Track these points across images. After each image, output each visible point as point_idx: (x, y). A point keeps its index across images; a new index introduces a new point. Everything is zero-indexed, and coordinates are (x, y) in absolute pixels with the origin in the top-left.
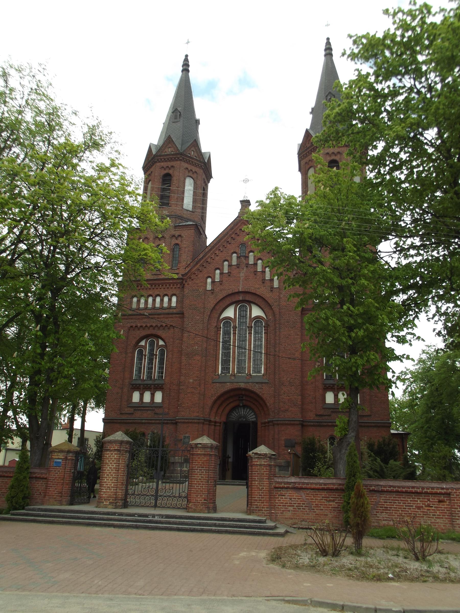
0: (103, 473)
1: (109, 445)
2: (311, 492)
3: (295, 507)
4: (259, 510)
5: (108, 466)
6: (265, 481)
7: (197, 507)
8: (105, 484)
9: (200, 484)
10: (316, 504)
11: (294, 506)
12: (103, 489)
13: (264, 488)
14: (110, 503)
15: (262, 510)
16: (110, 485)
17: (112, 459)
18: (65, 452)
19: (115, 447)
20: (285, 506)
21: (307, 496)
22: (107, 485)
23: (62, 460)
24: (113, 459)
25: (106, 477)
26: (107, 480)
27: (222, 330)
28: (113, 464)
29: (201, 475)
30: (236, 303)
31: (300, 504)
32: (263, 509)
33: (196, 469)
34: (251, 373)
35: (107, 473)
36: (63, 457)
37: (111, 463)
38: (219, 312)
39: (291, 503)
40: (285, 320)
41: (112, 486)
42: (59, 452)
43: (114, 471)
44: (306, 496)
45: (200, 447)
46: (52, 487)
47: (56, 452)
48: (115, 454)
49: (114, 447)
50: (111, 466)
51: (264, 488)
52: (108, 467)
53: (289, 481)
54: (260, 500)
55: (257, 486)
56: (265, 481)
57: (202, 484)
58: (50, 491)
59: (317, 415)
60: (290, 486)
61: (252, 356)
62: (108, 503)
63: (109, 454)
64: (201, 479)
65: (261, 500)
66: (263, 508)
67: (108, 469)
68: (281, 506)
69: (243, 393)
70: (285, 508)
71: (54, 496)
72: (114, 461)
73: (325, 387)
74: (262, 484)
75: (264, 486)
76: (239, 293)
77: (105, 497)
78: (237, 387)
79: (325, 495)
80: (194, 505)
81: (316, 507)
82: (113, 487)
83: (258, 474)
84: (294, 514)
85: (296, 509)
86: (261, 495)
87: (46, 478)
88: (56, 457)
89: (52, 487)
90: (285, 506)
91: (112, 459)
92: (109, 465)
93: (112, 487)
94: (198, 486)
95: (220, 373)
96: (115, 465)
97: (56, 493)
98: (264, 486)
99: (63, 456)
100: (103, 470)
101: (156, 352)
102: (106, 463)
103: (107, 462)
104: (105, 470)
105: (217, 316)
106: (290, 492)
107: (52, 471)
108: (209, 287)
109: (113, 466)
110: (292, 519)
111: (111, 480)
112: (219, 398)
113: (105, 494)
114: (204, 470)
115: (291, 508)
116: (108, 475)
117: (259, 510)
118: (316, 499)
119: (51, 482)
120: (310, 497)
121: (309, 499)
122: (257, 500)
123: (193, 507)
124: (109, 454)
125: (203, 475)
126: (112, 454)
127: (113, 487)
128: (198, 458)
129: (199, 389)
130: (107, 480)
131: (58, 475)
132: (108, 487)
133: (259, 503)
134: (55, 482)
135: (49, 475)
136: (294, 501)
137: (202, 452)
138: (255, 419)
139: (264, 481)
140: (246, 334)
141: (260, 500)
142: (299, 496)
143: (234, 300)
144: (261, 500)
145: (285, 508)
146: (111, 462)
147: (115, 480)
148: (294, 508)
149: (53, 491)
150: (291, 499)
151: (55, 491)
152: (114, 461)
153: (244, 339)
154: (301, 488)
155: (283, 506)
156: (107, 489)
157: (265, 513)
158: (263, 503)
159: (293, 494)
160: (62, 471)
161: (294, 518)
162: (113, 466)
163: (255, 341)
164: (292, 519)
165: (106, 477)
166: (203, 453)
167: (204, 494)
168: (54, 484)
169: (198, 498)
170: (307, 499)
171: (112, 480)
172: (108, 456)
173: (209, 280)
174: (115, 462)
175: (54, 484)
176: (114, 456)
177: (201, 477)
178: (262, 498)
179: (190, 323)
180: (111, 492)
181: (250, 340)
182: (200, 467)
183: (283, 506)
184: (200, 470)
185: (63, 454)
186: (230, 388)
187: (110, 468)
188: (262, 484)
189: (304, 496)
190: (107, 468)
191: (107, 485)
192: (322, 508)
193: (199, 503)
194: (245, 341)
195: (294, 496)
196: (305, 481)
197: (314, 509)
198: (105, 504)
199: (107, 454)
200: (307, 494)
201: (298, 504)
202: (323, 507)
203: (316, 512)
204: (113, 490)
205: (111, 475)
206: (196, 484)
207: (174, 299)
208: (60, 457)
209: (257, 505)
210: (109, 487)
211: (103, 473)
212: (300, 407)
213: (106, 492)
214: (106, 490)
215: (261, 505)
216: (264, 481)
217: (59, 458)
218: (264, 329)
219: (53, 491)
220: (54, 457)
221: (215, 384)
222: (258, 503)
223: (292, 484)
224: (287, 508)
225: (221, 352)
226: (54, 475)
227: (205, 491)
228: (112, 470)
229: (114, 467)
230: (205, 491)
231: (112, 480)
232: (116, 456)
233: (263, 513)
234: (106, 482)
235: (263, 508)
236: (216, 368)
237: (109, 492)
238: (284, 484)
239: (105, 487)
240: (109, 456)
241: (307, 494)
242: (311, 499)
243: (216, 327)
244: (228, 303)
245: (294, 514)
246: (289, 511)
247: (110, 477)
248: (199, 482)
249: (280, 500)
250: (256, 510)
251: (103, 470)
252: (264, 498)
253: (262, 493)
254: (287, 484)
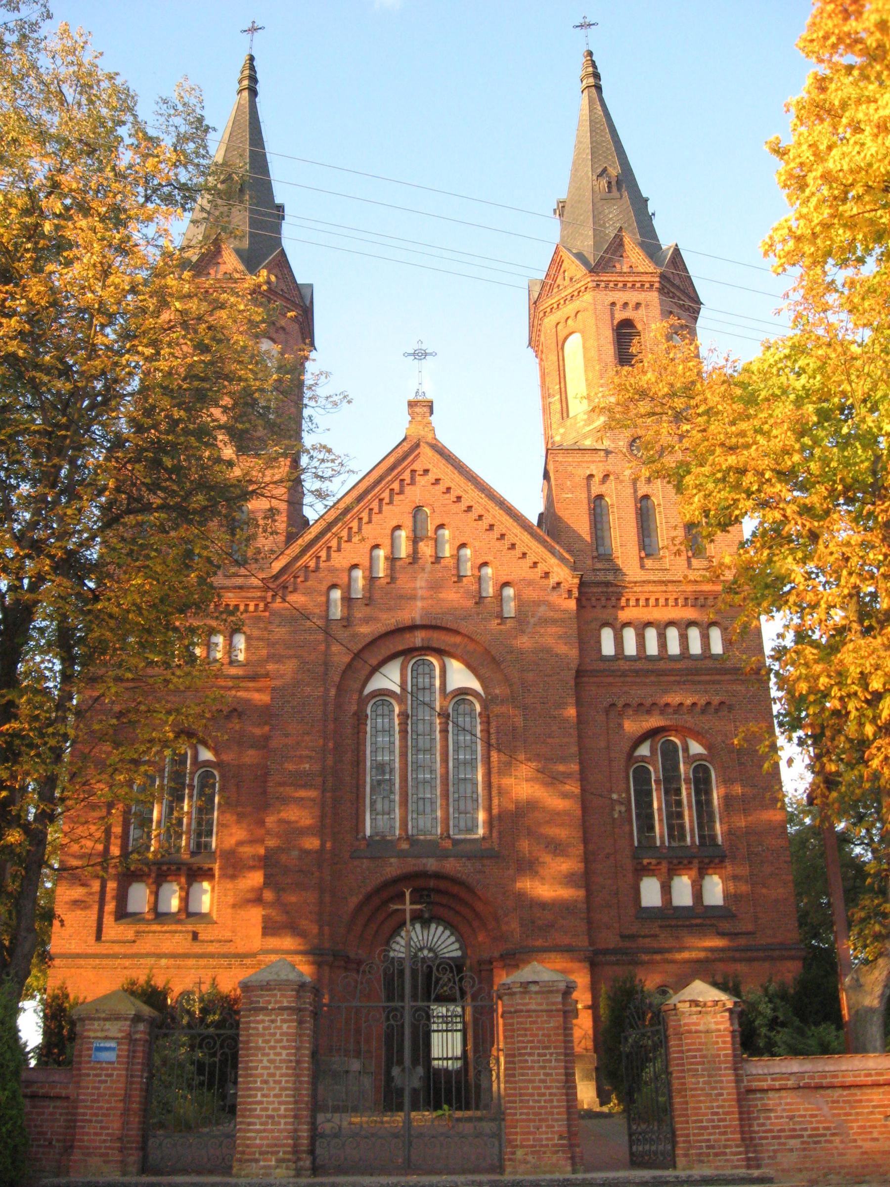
0: (251, 1075)
1: (262, 996)
2: (841, 1096)
3: (805, 1139)
4: (716, 1154)
5: (264, 1055)
6: (725, 1075)
7: (539, 1159)
8: (258, 1107)
9: (544, 1095)
10: (860, 1127)
11: (802, 1136)
12: (254, 1124)
13: (722, 1094)
14: (279, 1161)
15: (725, 1154)
16: (274, 1109)
17: (275, 1034)
18: (126, 1019)
19: (280, 1002)
20: (779, 1137)
21: (836, 1108)
22: (267, 1109)
23: (119, 1044)
24: (278, 1037)
25: (261, 1089)
26: (263, 1096)
27: (369, 722)
28: (278, 1050)
29: (544, 1068)
30: (407, 653)
31: (817, 1129)
32: (728, 1150)
33: (530, 1054)
34: (451, 833)
35: (262, 1075)
36: (120, 1035)
37: (274, 1048)
38: (363, 677)
39: (794, 1130)
40: (534, 697)
41: (282, 1112)
42: (105, 1019)
43: (284, 1071)
44: (832, 1108)
45: (536, 993)
46: (91, 1121)
47: (99, 1019)
48: (283, 1021)
49: (276, 1002)
50: (272, 1057)
51: (722, 1094)
52: (265, 1059)
53: (784, 1070)
54: (714, 1127)
55: (703, 1089)
56: (725, 1075)
57: (551, 1094)
58: (88, 1134)
59: (623, 937)
60: (790, 1083)
61: (451, 789)
62: (273, 1163)
63: (263, 1021)
64: (544, 1081)
65: (718, 1127)
66: (725, 1146)
67: (265, 1063)
68: (766, 1138)
69: (432, 883)
70: (780, 1144)
71: (100, 1148)
72: (281, 1041)
73: (639, 867)
74: (716, 1082)
75: (722, 1088)
76: (413, 628)
77: (261, 1146)
78: (416, 868)
79: (881, 1100)
80: (533, 1153)
81: (860, 1134)
82: (285, 1117)
83: (701, 1057)
84: (805, 1157)
85: (808, 1143)
86: (717, 1114)
87: (67, 1098)
88: (99, 1034)
89: (91, 1121)
90: (779, 1137)
91: (275, 1034)
92: (268, 1054)
93: (279, 1116)
94: (539, 1101)
95: (368, 832)
96: (284, 1052)
97: (105, 1141)
98: (722, 1088)
99: (121, 1031)
100: (251, 1068)
101: (192, 779)
102: (258, 1048)
103: (260, 1044)
104: (256, 1068)
105: (357, 686)
106: (789, 1100)
107: (88, 1075)
108: (337, 612)
109: (279, 1054)
110: (800, 1170)
111: (275, 1096)
112: (368, 898)
113: (262, 1138)
114: (551, 1054)
115: (792, 1143)
116: (266, 1082)
117: (716, 1154)
118: (857, 1114)
119: (86, 1107)
120: (842, 1108)
121: (839, 1115)
122: (706, 1128)
123: (530, 1158)
124: (263, 1021)
125: (550, 1068)
126: (272, 1021)
127: (285, 1117)
128: (532, 1023)
129: (317, 874)
130: (263, 1096)
131: (106, 1088)
132: (269, 1117)
133: (714, 1134)
134: (101, 1108)
135: (79, 1087)
136: (800, 1123)
137: (541, 1004)
138: (458, 953)
139: (720, 1075)
140: (432, 731)
141: (714, 1127)
142: (812, 1109)
143: (401, 647)
144: (718, 1127)
145: (780, 1144)
146: (272, 1044)
147: (287, 1096)
148: (803, 1143)
149: (96, 1134)
150: (791, 1118)
151: (101, 1134)
152: (281, 1041)
153: (428, 746)
154: (819, 1087)
155: (774, 1138)
156: (266, 1124)
157: (732, 1161)
158: (725, 1133)
159: (798, 1104)
160: (118, 1075)
161: (807, 1169)
162: (279, 1054)
163: (456, 750)
164: (800, 1170)
165: (261, 1089)
166: (544, 1007)
167: (557, 1120)
168: (96, 1115)
169: (541, 1133)
170: (834, 1115)
171: (280, 1096)
172: (260, 1026)
173: (336, 594)
174: (285, 1043)
175: (96, 1115)
176: (280, 1028)
177: (546, 1074)
178: (719, 1120)
179: (289, 702)
180: (280, 1131)
181: (445, 747)
182: (538, 1048)
183: (774, 1138)
184: (539, 1055)
185: (120, 1024)
186: (399, 872)
187: (270, 1061)
188: (716, 1082)
189: (825, 1109)
190: (261, 1061)
191: (267, 1109)
192: (875, 1135)
193: (547, 1146)
194: (430, 750)
195: (799, 1110)
196: (827, 1069)
197: (855, 1141)
198: (264, 1167)
199: (258, 1022)
200: (833, 1102)
201: (813, 1129)
202: (880, 1133)
203: (860, 1147)
204: (286, 1123)
205: (275, 1082)
206: (532, 1095)
207: (240, 642)
208: (111, 1035)
209: (709, 1140)
210: (272, 1117)
211: (251, 1075)
212: (583, 915)
213: (265, 1131)
214: (261, 1124)
215: (720, 1140)
216: (720, 1075)
217: (106, 1038)
218: (478, 720)
219: (96, 1134)
220: (92, 1034)
221: (356, 862)
222: (710, 1134)
223: (793, 1078)
224: (784, 1144)
225: (368, 780)
226: (94, 1088)
227: (558, 1114)
228: (277, 1068)
229: (284, 1057)
230: (558, 1114)
231: (280, 1096)
232: (285, 1026)
233: (727, 1160)
234: (261, 1103)
235: (725, 1146)
236: (357, 818)
237: (272, 1131)
238: (773, 1080)
239: (259, 1117)
240: (265, 1028)
241: (833, 1102)
242: (846, 1114)
243: (355, 714)
244: (384, 652)
245: (805, 1157)
246: (791, 1150)
247: (274, 1088)
248: (539, 1088)
249: (763, 1125)
250: (708, 1155)
251: (251, 1068)
252: (724, 1120)
253: (718, 1107)
254: (781, 1079)
